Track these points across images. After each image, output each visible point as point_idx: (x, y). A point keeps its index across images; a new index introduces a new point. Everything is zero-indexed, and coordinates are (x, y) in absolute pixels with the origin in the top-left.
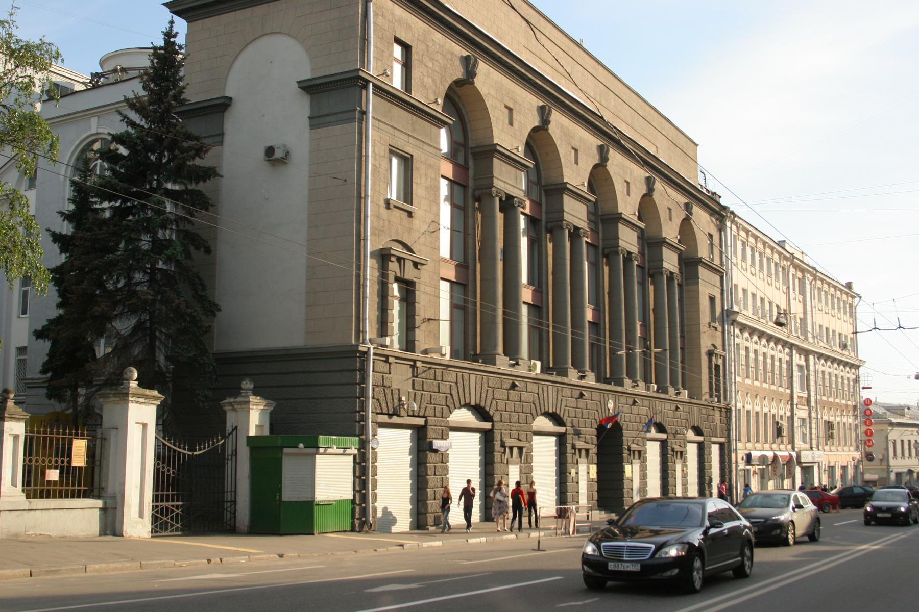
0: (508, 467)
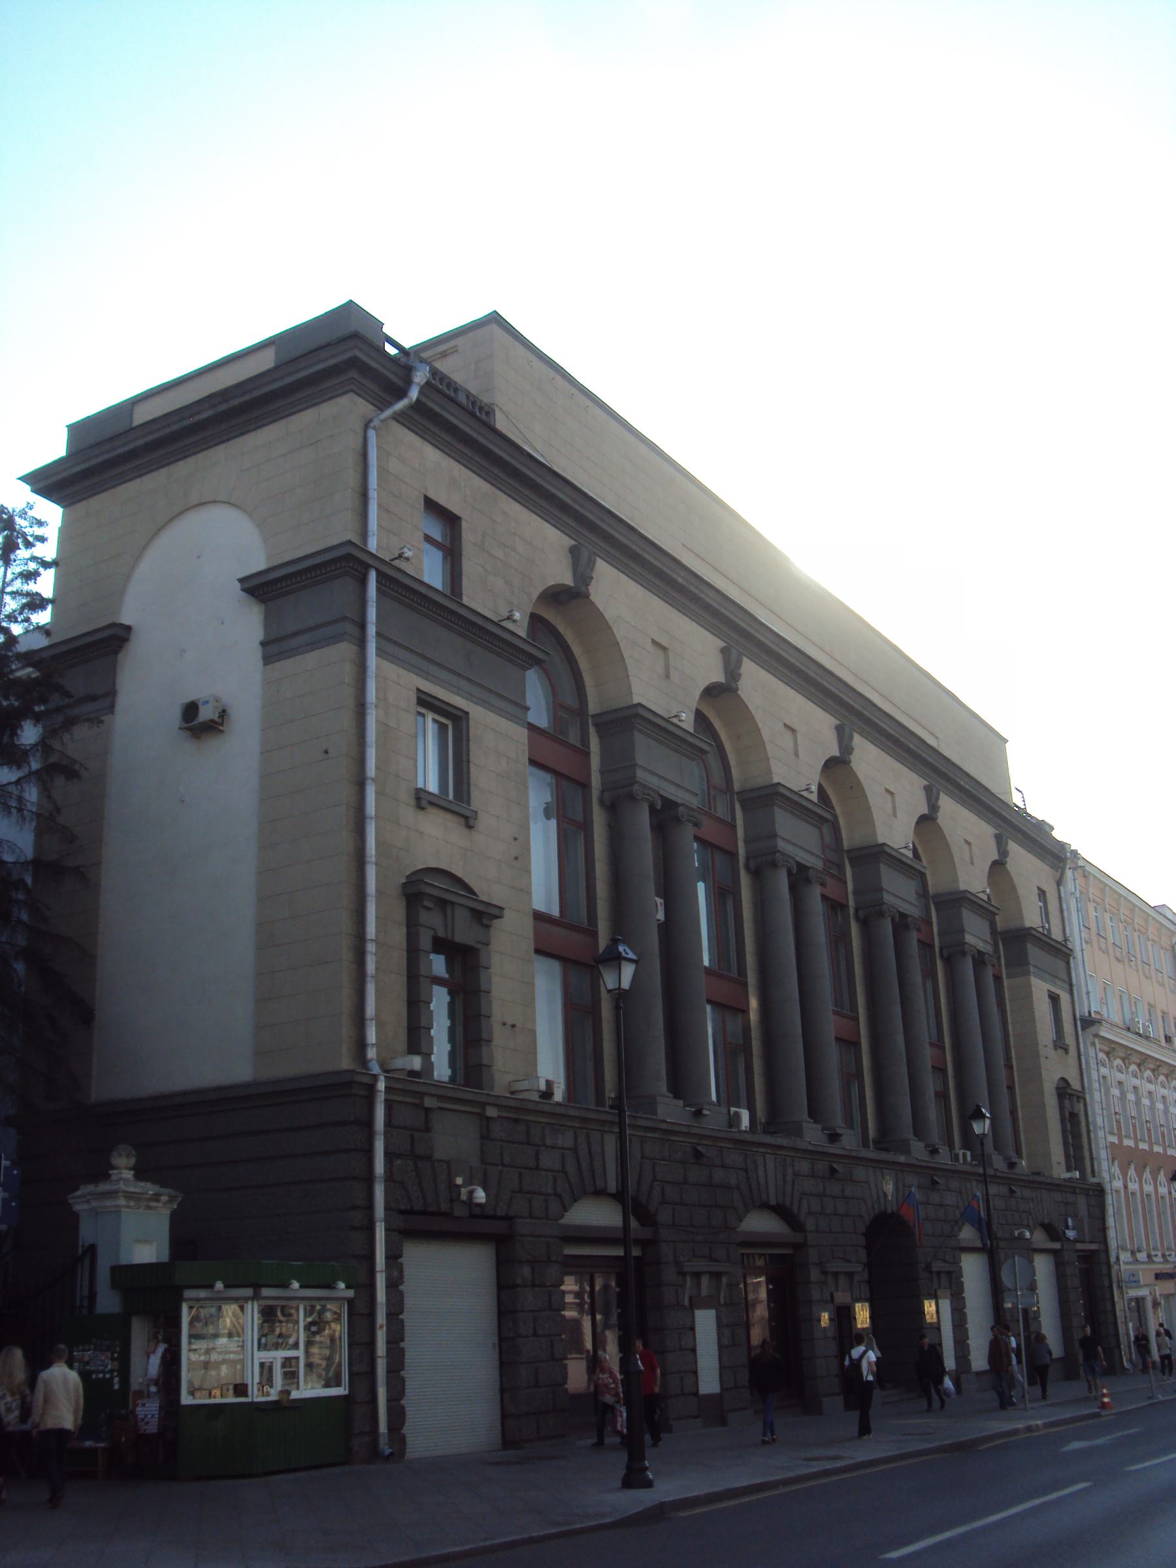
0: (693, 1313)
